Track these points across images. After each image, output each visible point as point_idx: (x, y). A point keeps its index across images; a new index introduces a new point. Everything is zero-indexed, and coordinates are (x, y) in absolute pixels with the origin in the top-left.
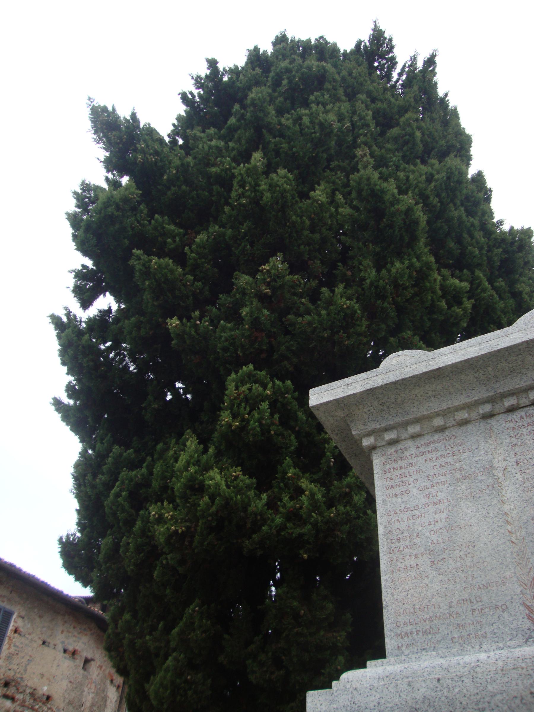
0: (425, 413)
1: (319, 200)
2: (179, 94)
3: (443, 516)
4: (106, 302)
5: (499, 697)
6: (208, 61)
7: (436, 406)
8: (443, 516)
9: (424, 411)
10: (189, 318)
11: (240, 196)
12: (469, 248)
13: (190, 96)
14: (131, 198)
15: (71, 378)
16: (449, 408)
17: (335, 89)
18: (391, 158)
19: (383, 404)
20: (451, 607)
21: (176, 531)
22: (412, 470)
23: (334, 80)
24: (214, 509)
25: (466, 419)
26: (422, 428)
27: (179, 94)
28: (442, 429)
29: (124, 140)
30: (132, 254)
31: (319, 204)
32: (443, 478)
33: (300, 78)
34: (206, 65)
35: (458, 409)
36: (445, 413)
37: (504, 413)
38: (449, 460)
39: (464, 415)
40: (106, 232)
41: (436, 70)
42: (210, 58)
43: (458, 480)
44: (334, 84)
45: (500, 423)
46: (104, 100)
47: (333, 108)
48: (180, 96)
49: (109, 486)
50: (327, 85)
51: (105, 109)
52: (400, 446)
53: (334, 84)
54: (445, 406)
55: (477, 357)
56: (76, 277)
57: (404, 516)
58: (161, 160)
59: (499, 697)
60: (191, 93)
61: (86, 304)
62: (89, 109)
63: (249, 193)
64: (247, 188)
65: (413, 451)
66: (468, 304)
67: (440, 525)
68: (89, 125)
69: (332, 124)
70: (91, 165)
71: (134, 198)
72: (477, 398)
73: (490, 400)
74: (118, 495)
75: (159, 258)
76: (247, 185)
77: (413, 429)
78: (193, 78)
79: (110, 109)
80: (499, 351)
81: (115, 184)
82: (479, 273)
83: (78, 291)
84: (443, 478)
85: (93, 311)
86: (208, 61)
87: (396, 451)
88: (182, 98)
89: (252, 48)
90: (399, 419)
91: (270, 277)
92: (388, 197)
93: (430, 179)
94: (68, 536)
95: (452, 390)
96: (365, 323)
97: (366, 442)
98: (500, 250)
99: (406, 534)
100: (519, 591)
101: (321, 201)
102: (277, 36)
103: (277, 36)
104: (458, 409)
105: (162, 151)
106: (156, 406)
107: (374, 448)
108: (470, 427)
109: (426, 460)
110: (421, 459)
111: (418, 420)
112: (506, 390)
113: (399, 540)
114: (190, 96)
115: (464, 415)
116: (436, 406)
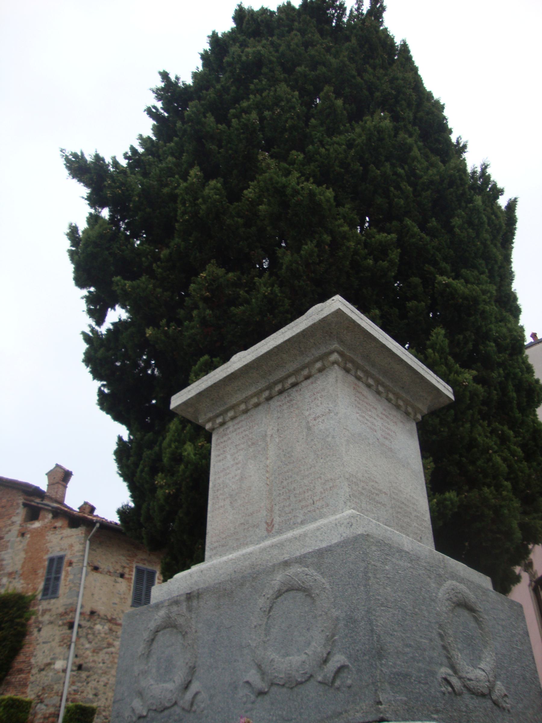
0: (235, 402)
1: (249, 198)
2: (145, 111)
3: (239, 471)
4: (117, 314)
5: (223, 576)
6: (160, 73)
7: (240, 397)
8: (239, 471)
9: (234, 401)
10: (159, 327)
11: (184, 213)
12: (396, 200)
13: (154, 110)
14: (105, 233)
15: (98, 384)
16: (247, 397)
17: (272, 70)
18: (316, 134)
19: (212, 400)
20: (235, 529)
21: (169, 493)
22: (230, 441)
23: (271, 62)
24: (188, 473)
25: (257, 403)
26: (235, 412)
27: (145, 111)
28: (246, 411)
29: (95, 180)
30: (112, 282)
31: (250, 201)
32: (242, 446)
33: (240, 69)
34: (159, 78)
35: (252, 396)
36: (246, 401)
37: (278, 395)
38: (247, 433)
39: (255, 400)
40: (97, 263)
41: (384, 4)
42: (162, 71)
43: (249, 446)
44: (271, 66)
45: (275, 403)
46: (74, 147)
47: (269, 93)
48: (146, 112)
49: (136, 465)
50: (265, 70)
51: (75, 155)
52: (226, 426)
53: (271, 66)
54: (244, 396)
55: (251, 362)
56: (87, 302)
57: (222, 474)
58: (127, 190)
59: (223, 576)
60: (155, 107)
61: (100, 321)
62: (64, 160)
63: (190, 209)
64: (187, 205)
65: (231, 429)
66: (395, 255)
67: (237, 478)
68: (66, 172)
69: (254, 123)
70: (75, 206)
71: (108, 232)
72: (260, 388)
73: (269, 388)
74: (142, 471)
75: (132, 281)
76: (187, 203)
77: (231, 414)
78: (153, 92)
79: (79, 154)
80: (262, 356)
81: (93, 219)
82: (408, 222)
83: (91, 313)
84: (242, 446)
85: (107, 325)
86: (160, 73)
87: (223, 430)
88: (148, 114)
89: (210, 34)
90: (222, 409)
91: (207, 282)
92: (289, 191)
93: (350, 145)
94: (122, 507)
95: (247, 384)
96: (287, 302)
97: (208, 426)
98: (429, 192)
99: (222, 486)
100: (265, 515)
101: (251, 198)
102: (236, 10)
103: (236, 10)
104: (252, 396)
105: (126, 181)
106: (162, 395)
107: (213, 429)
108: (260, 408)
109: (236, 434)
110: (234, 434)
111: (233, 407)
112: (274, 380)
113: (218, 490)
114: (154, 110)
115: (255, 400)
116: (240, 397)
